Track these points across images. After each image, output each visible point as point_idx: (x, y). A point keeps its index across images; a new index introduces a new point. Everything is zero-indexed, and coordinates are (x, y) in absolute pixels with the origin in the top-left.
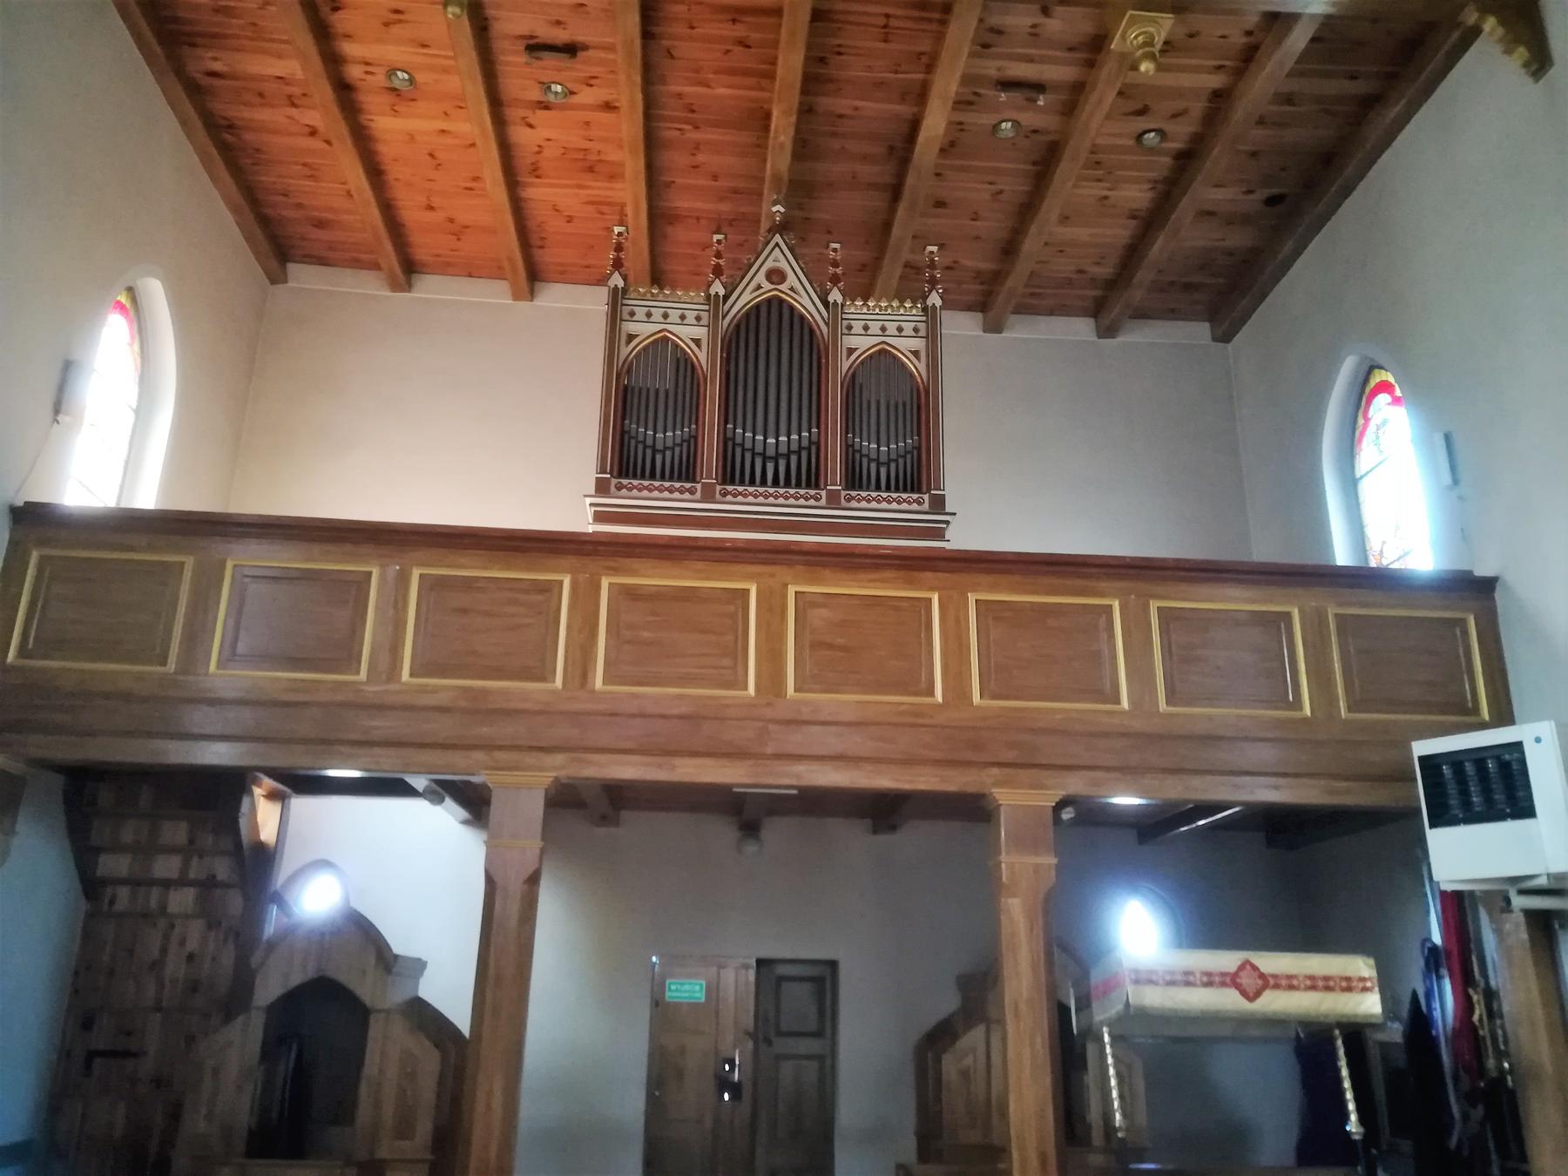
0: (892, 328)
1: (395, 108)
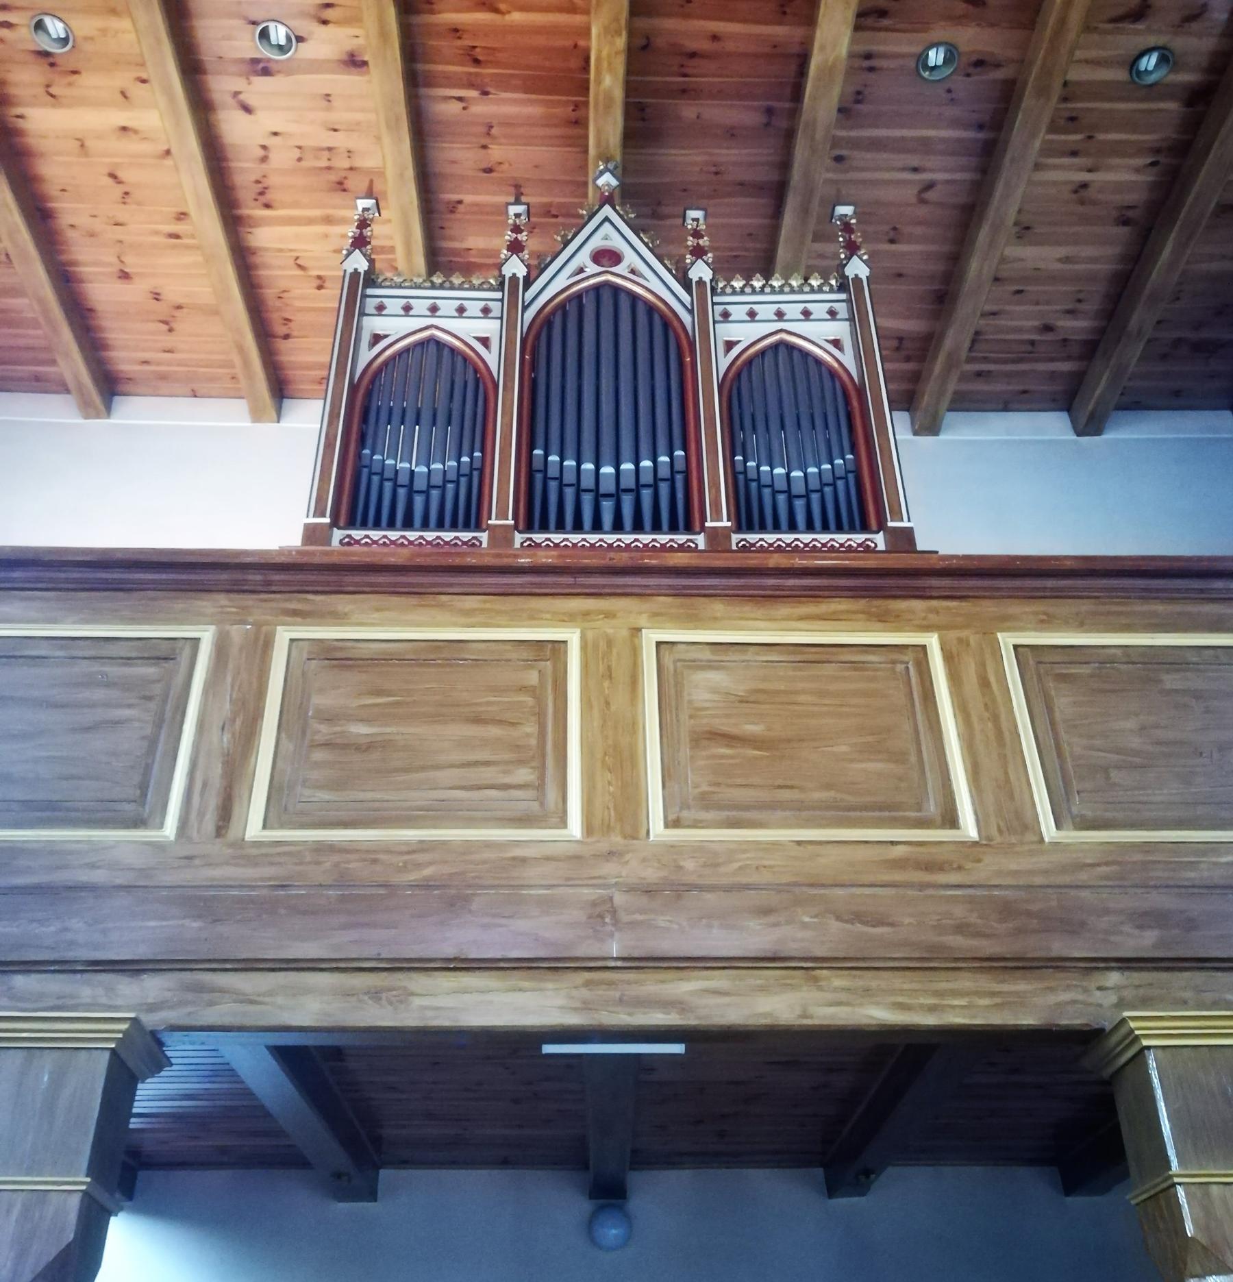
0: (793, 311)
1: (53, 90)
